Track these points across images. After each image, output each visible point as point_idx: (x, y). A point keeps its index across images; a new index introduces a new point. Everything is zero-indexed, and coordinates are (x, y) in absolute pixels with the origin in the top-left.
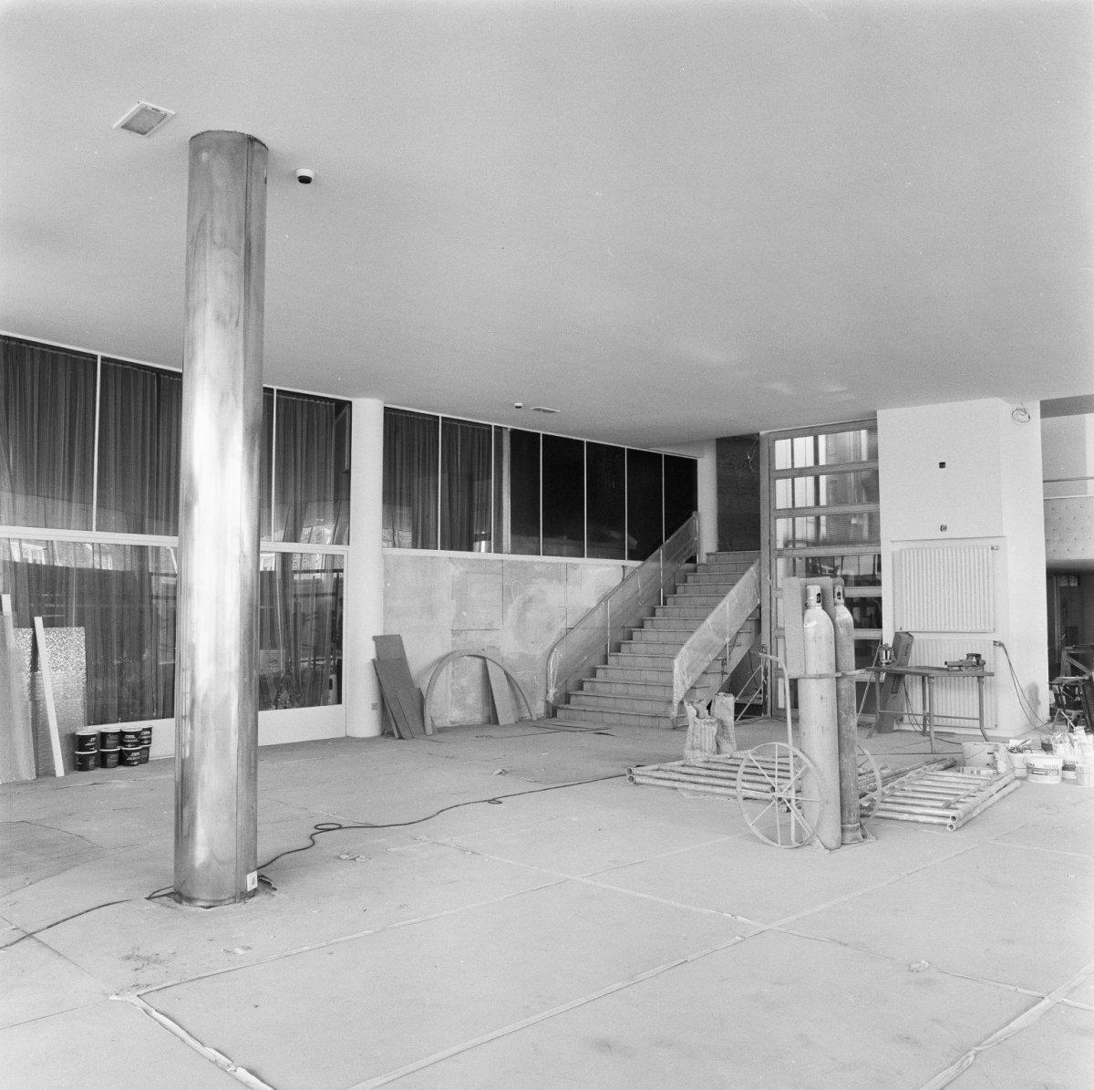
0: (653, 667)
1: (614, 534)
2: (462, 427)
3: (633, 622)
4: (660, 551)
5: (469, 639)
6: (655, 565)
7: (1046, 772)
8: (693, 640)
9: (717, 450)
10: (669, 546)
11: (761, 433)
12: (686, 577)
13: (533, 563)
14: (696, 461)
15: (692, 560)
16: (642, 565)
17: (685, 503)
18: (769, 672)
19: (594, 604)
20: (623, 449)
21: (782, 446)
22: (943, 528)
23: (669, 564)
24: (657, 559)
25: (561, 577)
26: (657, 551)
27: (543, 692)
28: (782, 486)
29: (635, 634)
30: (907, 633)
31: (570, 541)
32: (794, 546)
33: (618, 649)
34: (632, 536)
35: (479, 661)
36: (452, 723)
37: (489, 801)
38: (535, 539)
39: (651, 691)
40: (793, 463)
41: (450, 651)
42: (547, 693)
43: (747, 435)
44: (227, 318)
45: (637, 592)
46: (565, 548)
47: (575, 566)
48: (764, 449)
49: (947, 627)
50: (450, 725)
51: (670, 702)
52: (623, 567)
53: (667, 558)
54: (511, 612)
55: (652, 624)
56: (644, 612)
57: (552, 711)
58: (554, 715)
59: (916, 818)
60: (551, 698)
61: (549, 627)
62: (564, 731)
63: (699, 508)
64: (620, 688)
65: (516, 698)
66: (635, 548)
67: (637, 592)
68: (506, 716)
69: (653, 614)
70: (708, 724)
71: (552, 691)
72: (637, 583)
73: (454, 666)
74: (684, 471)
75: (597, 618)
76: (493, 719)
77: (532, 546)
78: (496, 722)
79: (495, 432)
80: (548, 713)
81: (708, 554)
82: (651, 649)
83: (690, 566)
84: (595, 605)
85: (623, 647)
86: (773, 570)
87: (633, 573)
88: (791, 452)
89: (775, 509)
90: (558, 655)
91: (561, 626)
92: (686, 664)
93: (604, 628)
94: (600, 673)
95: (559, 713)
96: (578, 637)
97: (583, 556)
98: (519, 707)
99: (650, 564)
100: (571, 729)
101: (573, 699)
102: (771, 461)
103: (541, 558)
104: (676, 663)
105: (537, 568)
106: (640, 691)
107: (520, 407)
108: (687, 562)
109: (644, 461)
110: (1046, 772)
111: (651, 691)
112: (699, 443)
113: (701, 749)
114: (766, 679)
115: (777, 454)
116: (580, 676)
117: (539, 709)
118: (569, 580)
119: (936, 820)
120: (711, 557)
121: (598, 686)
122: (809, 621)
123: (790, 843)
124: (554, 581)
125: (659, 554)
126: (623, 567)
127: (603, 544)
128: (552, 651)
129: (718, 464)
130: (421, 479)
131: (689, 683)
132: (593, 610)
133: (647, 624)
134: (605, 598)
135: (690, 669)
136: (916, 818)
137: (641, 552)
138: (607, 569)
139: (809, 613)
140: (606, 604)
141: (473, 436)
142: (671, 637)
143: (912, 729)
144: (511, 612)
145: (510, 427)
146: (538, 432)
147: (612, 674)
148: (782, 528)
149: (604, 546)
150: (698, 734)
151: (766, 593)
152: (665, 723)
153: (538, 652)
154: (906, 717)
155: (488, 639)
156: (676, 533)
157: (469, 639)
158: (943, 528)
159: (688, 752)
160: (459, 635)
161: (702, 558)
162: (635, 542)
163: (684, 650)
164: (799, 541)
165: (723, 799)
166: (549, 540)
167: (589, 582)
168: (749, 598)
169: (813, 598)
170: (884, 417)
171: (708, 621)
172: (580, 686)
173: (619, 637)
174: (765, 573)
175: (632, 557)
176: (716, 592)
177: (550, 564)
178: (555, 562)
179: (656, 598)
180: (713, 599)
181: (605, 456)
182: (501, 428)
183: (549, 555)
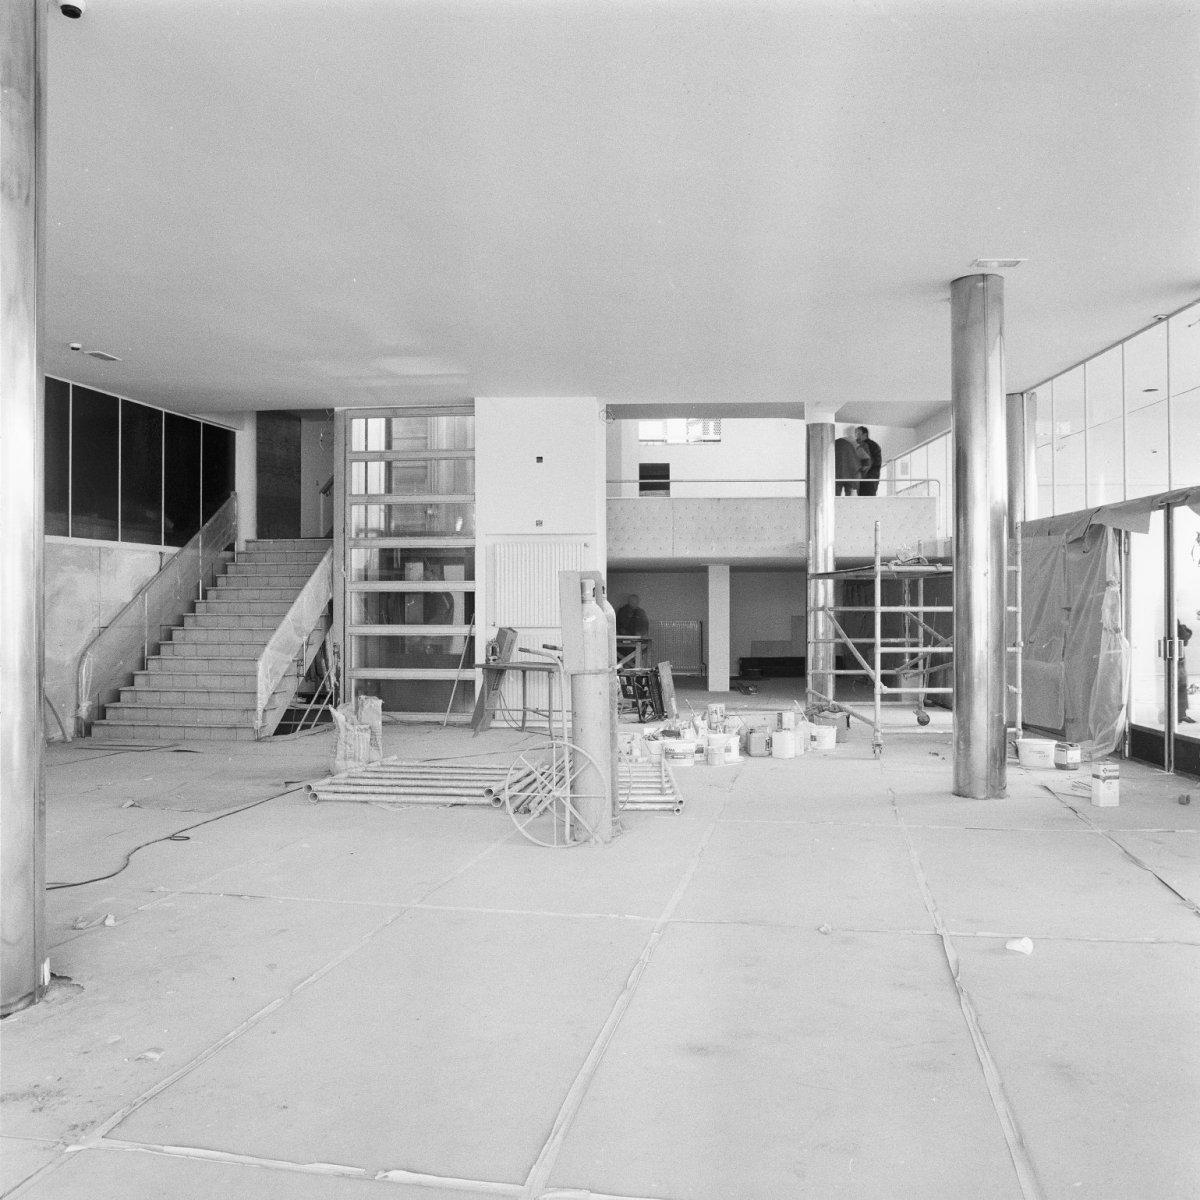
0: (208, 671)
1: (150, 514)
4: (199, 537)
6: (195, 552)
7: (684, 755)
8: (275, 640)
9: (257, 423)
10: (208, 531)
11: (336, 409)
13: (63, 546)
14: (234, 433)
15: (231, 548)
18: (342, 672)
19: (128, 598)
20: (161, 412)
21: (358, 425)
22: (539, 523)
25: (93, 564)
26: (195, 537)
27: (73, 705)
28: (357, 469)
30: (510, 628)
32: (366, 536)
33: (156, 650)
34: (170, 518)
37: (172, 838)
40: (366, 446)
43: (294, 411)
44: (15, 191)
47: (109, 551)
48: (339, 424)
49: (536, 622)
52: (161, 553)
55: (196, 621)
56: (181, 609)
57: (85, 729)
58: (89, 733)
59: (638, 806)
60: (84, 713)
62: (128, 750)
63: (237, 489)
64: (172, 698)
70: (361, 731)
71: (85, 705)
72: (174, 574)
74: (221, 442)
81: (248, 542)
83: (228, 554)
85: (163, 649)
86: (348, 560)
88: (366, 434)
90: (91, 659)
92: (270, 667)
93: (141, 627)
94: (139, 680)
95: (94, 730)
96: (112, 637)
97: (116, 539)
99: (189, 551)
100: (136, 749)
101: (109, 713)
102: (347, 443)
103: (70, 540)
104: (260, 665)
105: (67, 552)
106: (203, 699)
107: (78, 349)
108: (226, 550)
109: (182, 428)
110: (684, 755)
111: (215, 699)
112: (238, 414)
113: (354, 758)
114: (338, 680)
116: (114, 686)
119: (658, 807)
120: (252, 545)
122: (588, 615)
123: (564, 842)
124: (86, 569)
126: (161, 553)
128: (84, 655)
129: (258, 438)
131: (272, 688)
132: (127, 607)
133: (188, 622)
135: (273, 672)
136: (638, 806)
137: (179, 535)
138: (142, 556)
139: (586, 605)
143: (505, 725)
147: (155, 681)
148: (356, 515)
149: (140, 530)
150: (351, 742)
151: (339, 586)
152: (247, 735)
154: (498, 714)
156: (216, 515)
158: (539, 523)
159: (339, 763)
161: (240, 546)
163: (267, 649)
165: (431, 807)
168: (324, 592)
169: (589, 592)
171: (289, 617)
172: (116, 697)
175: (169, 543)
177: (82, 548)
178: (87, 545)
181: (141, 417)
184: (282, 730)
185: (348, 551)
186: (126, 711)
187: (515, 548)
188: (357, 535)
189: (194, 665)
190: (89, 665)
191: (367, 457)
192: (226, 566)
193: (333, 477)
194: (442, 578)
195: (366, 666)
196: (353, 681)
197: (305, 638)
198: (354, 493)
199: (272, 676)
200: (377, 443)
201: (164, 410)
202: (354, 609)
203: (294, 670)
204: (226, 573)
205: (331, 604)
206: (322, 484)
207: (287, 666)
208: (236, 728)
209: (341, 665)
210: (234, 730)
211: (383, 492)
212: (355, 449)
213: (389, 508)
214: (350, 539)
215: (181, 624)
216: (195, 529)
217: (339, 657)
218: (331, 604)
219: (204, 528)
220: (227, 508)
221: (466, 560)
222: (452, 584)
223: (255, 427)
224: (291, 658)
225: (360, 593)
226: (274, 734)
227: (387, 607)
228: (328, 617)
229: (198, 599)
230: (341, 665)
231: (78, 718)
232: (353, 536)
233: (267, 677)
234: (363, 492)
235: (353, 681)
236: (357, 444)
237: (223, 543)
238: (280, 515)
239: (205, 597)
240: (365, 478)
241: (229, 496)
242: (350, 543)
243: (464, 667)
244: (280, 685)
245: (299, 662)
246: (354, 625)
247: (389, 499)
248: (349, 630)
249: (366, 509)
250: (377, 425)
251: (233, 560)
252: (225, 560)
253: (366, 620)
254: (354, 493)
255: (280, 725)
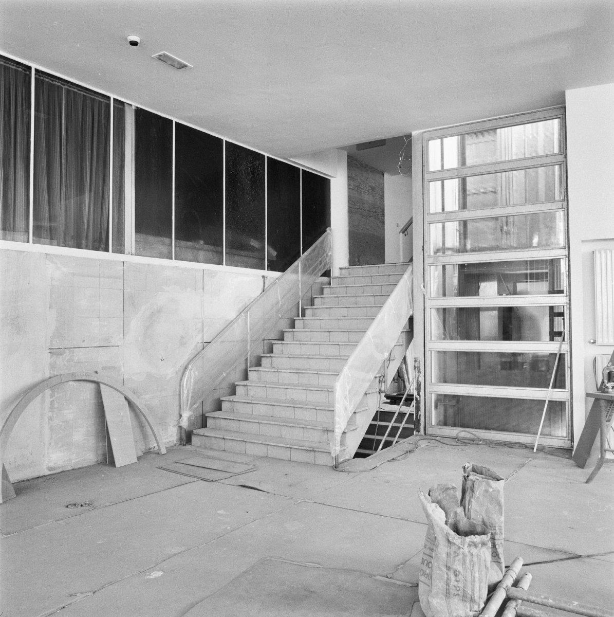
1: (254, 243)
2: (68, 91)
3: (273, 335)
4: (298, 264)
5: (76, 359)
6: (294, 277)
8: (356, 356)
9: (348, 172)
10: (307, 259)
11: (414, 133)
12: (322, 289)
15: (327, 274)
16: (282, 276)
17: (318, 220)
19: (232, 315)
21: (434, 146)
23: (306, 277)
24: (296, 271)
26: (296, 263)
27: (176, 417)
28: (434, 188)
29: (275, 347)
31: (207, 247)
33: (258, 363)
35: (92, 386)
36: (50, 469)
38: (167, 240)
39: (300, 414)
41: (47, 375)
42: (181, 416)
45: (278, 303)
46: (202, 254)
50: (48, 473)
51: (329, 431)
52: (263, 277)
53: (304, 271)
54: (135, 324)
56: (283, 325)
60: (185, 423)
61: (183, 343)
64: (262, 410)
65: (142, 427)
66: (275, 259)
67: (278, 303)
68: (125, 454)
69: (293, 326)
70: (475, 545)
71: (186, 415)
73: (52, 396)
74: (318, 187)
75: (237, 332)
76: (108, 459)
77: (164, 250)
78: (112, 463)
79: (114, 107)
80: (181, 439)
81: (341, 269)
82: (296, 363)
83: (325, 279)
84: (235, 317)
85: (264, 361)
87: (273, 284)
88: (441, 153)
89: (429, 214)
91: (198, 339)
92: (348, 388)
93: (244, 341)
95: (195, 440)
98: (145, 437)
101: (210, 422)
103: (173, 263)
106: (288, 413)
111: (300, 414)
115: (430, 159)
117: (169, 436)
118: (206, 288)
120: (344, 271)
121: (238, 406)
125: (298, 266)
126: (263, 277)
127: (242, 253)
128: (186, 368)
129: (349, 185)
130: (63, 202)
131: (351, 409)
133: (288, 336)
134: (245, 310)
137: (281, 263)
140: (246, 316)
141: (84, 106)
142: (332, 351)
144: (135, 324)
145: (135, 104)
146: (171, 118)
148: (434, 232)
149: (242, 252)
152: (322, 459)
153: (170, 371)
155: (103, 358)
157: (76, 359)
160: (61, 354)
161: (335, 273)
162: (275, 253)
164: (448, 249)
166: (183, 243)
167: (228, 292)
170: (572, 97)
171: (369, 333)
173: (259, 352)
174: (418, 281)
176: (356, 303)
179: (295, 310)
180: (374, 309)
182: (123, 103)
183: (182, 259)
184: (367, 447)
185: (427, 267)
186: (223, 422)
187: (603, 254)
188: (435, 253)
189: (286, 377)
190: (190, 377)
191: (442, 176)
192: (323, 288)
193: (412, 218)
194: (515, 293)
195: (445, 382)
196: (433, 395)
197: (386, 355)
198: (432, 211)
199: (351, 401)
200: (452, 162)
201: (266, 155)
202: (434, 323)
203: (377, 386)
204: (323, 294)
205: (411, 320)
206: (402, 226)
207: (368, 385)
208: (315, 451)
209: (421, 379)
210: (312, 453)
211: (457, 209)
212: (432, 169)
213: (464, 224)
214: (429, 256)
215: (282, 339)
216: (296, 256)
217: (419, 372)
218: (411, 320)
219: (303, 256)
220: (323, 240)
221: (547, 273)
222: (533, 299)
223: (346, 170)
224: (371, 376)
225: (438, 310)
226: (354, 458)
227: (464, 323)
228: (410, 333)
229: (299, 316)
230: (421, 379)
231: (180, 427)
232: (432, 254)
233: (345, 397)
234: (440, 210)
235: (433, 395)
236: (434, 164)
237: (320, 270)
238: (367, 247)
239: (303, 315)
240: (442, 197)
241: (325, 231)
242: (428, 261)
243: (554, 387)
244: (360, 405)
245: (381, 379)
246: (436, 342)
247: (466, 215)
248: (428, 346)
249: (444, 228)
250: (452, 143)
251: (330, 284)
252: (322, 284)
253: (447, 335)
254: (432, 211)
255: (364, 440)
